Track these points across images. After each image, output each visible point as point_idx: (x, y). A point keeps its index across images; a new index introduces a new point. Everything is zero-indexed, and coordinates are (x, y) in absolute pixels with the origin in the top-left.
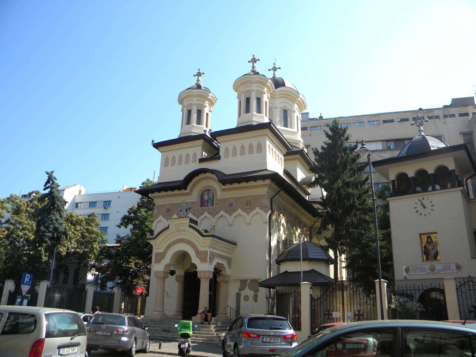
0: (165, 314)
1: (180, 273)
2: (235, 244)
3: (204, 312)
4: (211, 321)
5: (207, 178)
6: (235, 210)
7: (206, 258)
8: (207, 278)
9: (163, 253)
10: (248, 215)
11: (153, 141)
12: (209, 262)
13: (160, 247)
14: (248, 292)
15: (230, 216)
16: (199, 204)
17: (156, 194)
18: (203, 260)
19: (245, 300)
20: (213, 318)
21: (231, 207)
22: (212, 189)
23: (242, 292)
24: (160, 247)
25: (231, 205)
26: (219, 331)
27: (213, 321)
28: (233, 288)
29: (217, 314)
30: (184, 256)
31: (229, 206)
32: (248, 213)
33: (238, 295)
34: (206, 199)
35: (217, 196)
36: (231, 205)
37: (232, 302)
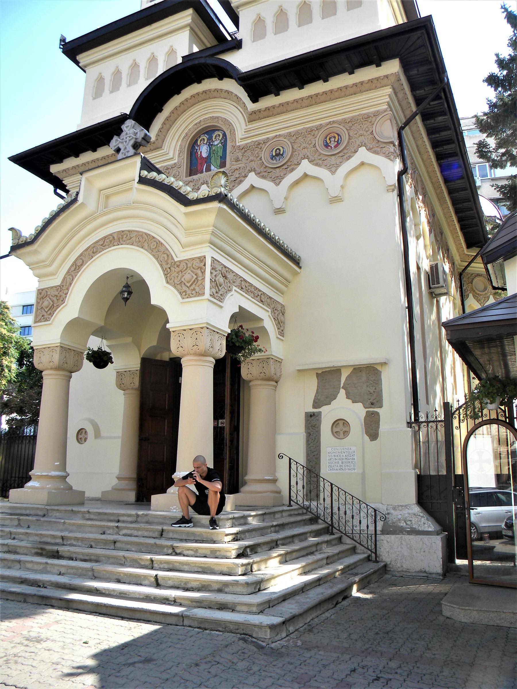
0: (71, 488)
1: (127, 361)
2: (296, 261)
3: (191, 475)
4: (220, 509)
5: (208, 95)
6: (289, 167)
7: (198, 281)
8: (204, 354)
9: (59, 288)
10: (333, 173)
11: (63, 40)
12: (212, 295)
13: (52, 269)
14: (344, 407)
15: (277, 185)
16: (184, 169)
17: (70, 163)
18: (188, 289)
19: (335, 434)
20: (230, 499)
21: (277, 161)
22: (220, 124)
23: (324, 410)
24: (52, 269)
25: (277, 155)
26: (254, 549)
27: (228, 507)
28: (294, 400)
29: (245, 483)
30: (130, 291)
31: (272, 157)
32: (333, 169)
33: (312, 421)
34: (204, 155)
35: (234, 140)
36: (277, 155)
37: (292, 444)
